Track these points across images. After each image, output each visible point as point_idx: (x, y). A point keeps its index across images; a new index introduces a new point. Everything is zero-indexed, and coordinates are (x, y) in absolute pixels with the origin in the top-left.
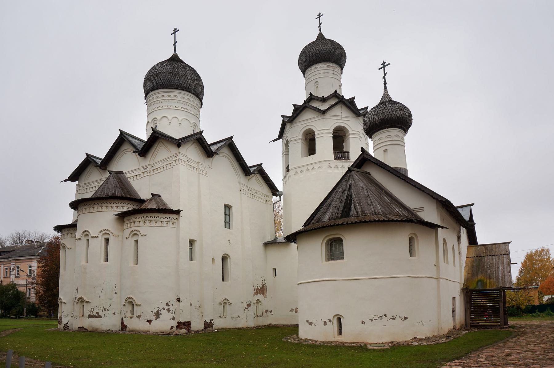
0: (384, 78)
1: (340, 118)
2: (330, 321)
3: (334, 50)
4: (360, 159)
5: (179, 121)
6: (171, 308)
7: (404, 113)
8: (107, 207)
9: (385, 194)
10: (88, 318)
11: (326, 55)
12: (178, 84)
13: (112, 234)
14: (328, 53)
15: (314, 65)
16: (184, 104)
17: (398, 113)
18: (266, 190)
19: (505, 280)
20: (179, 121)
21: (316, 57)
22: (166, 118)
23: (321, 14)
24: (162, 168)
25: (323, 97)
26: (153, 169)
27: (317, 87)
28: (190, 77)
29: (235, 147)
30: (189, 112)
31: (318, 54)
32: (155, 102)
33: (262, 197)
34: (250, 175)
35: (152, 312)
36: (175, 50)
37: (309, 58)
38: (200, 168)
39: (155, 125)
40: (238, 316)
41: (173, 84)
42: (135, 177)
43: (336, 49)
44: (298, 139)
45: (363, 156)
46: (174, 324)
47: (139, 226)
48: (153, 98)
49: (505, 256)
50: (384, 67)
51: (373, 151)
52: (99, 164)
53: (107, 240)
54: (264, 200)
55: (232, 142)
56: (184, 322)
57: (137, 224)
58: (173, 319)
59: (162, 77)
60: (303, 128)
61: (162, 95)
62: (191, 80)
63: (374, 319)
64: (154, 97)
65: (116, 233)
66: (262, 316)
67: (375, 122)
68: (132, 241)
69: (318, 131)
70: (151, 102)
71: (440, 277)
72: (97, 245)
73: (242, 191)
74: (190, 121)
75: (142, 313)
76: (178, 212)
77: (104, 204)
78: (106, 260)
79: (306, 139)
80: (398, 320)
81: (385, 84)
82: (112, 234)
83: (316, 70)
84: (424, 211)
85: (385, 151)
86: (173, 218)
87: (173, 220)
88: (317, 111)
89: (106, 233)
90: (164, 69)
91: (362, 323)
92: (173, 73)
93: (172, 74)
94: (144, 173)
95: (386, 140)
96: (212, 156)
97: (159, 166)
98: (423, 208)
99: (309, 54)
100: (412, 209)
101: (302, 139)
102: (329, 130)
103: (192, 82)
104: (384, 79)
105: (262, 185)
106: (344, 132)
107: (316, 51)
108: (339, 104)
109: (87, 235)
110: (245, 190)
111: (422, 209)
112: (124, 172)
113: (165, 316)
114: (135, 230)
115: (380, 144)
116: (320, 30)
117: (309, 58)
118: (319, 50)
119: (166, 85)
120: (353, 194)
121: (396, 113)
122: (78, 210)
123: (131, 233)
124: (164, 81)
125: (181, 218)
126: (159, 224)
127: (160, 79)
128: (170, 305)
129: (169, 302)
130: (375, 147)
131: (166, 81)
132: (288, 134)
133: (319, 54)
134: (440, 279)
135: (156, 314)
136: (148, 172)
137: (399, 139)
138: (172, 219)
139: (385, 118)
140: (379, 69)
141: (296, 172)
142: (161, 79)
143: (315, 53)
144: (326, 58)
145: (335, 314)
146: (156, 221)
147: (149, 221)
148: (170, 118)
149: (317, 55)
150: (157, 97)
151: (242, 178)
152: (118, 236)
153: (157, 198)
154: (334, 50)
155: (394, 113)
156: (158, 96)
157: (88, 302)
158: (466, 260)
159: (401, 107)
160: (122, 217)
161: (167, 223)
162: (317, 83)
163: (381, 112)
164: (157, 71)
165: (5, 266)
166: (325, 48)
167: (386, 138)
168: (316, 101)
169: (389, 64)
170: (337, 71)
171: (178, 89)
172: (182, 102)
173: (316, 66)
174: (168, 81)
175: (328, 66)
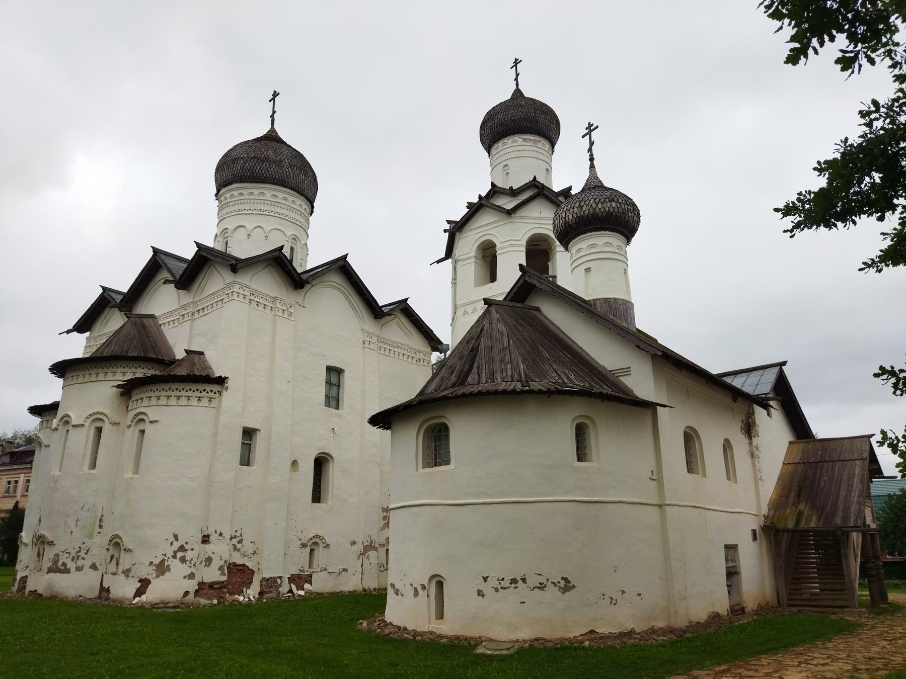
1: (538, 221)
2: (423, 587)
4: (519, 285)
5: (265, 233)
6: (189, 555)
7: (618, 205)
8: (106, 373)
10: (47, 573)
11: (522, 122)
12: (266, 176)
13: (109, 419)
15: (502, 139)
16: (262, 203)
17: (606, 205)
18: (417, 342)
20: (265, 233)
21: (505, 126)
22: (243, 228)
26: (198, 309)
28: (287, 164)
29: (352, 272)
30: (285, 218)
31: (508, 122)
32: (229, 204)
33: (409, 354)
34: (383, 317)
35: (151, 563)
37: (494, 129)
38: (279, 306)
39: (226, 240)
41: (258, 175)
43: (538, 112)
44: (469, 258)
45: (525, 280)
46: (192, 585)
47: (158, 404)
48: (226, 197)
50: (589, 133)
52: (118, 302)
53: (99, 430)
54: (415, 360)
55: (345, 263)
56: (211, 583)
58: (191, 576)
59: (240, 164)
60: (477, 240)
62: (290, 169)
63: (502, 588)
64: (228, 195)
65: (115, 419)
68: (134, 432)
69: (501, 243)
70: (223, 204)
71: (668, 502)
72: (81, 440)
73: (367, 345)
74: (285, 232)
77: (101, 369)
78: (93, 466)
79: (484, 257)
80: (552, 592)
81: (592, 159)
82: (109, 419)
84: (630, 374)
85: (588, 270)
86: (212, 391)
87: (211, 395)
88: (499, 211)
89: (97, 419)
90: (245, 153)
91: (479, 595)
92: (258, 158)
94: (184, 315)
95: (587, 253)
96: (302, 287)
97: (207, 305)
100: (610, 371)
101: (476, 257)
102: (519, 240)
103: (291, 171)
106: (549, 243)
107: (504, 117)
110: (373, 343)
111: (627, 371)
112: (156, 315)
113: (178, 569)
114: (141, 413)
115: (580, 259)
116: (517, 85)
117: (494, 129)
118: (509, 116)
120: (483, 345)
124: (244, 171)
125: (224, 393)
126: (183, 401)
127: (237, 169)
128: (187, 550)
129: (187, 543)
130: (573, 264)
132: (457, 252)
134: (666, 507)
136: (190, 314)
137: (612, 250)
138: (209, 392)
139: (584, 216)
141: (465, 311)
143: (503, 121)
144: (522, 126)
147: (167, 396)
148: (250, 227)
150: (232, 196)
151: (368, 323)
152: (119, 424)
153: (196, 359)
154: (534, 115)
155: (600, 206)
156: (232, 194)
157: (51, 543)
158: (782, 469)
160: (128, 390)
161: (199, 399)
163: (577, 204)
164: (233, 155)
165: (26, 477)
166: (519, 111)
167: (604, 246)
168: (502, 195)
169: (598, 126)
170: (542, 147)
172: (273, 203)
173: (505, 140)
175: (525, 140)
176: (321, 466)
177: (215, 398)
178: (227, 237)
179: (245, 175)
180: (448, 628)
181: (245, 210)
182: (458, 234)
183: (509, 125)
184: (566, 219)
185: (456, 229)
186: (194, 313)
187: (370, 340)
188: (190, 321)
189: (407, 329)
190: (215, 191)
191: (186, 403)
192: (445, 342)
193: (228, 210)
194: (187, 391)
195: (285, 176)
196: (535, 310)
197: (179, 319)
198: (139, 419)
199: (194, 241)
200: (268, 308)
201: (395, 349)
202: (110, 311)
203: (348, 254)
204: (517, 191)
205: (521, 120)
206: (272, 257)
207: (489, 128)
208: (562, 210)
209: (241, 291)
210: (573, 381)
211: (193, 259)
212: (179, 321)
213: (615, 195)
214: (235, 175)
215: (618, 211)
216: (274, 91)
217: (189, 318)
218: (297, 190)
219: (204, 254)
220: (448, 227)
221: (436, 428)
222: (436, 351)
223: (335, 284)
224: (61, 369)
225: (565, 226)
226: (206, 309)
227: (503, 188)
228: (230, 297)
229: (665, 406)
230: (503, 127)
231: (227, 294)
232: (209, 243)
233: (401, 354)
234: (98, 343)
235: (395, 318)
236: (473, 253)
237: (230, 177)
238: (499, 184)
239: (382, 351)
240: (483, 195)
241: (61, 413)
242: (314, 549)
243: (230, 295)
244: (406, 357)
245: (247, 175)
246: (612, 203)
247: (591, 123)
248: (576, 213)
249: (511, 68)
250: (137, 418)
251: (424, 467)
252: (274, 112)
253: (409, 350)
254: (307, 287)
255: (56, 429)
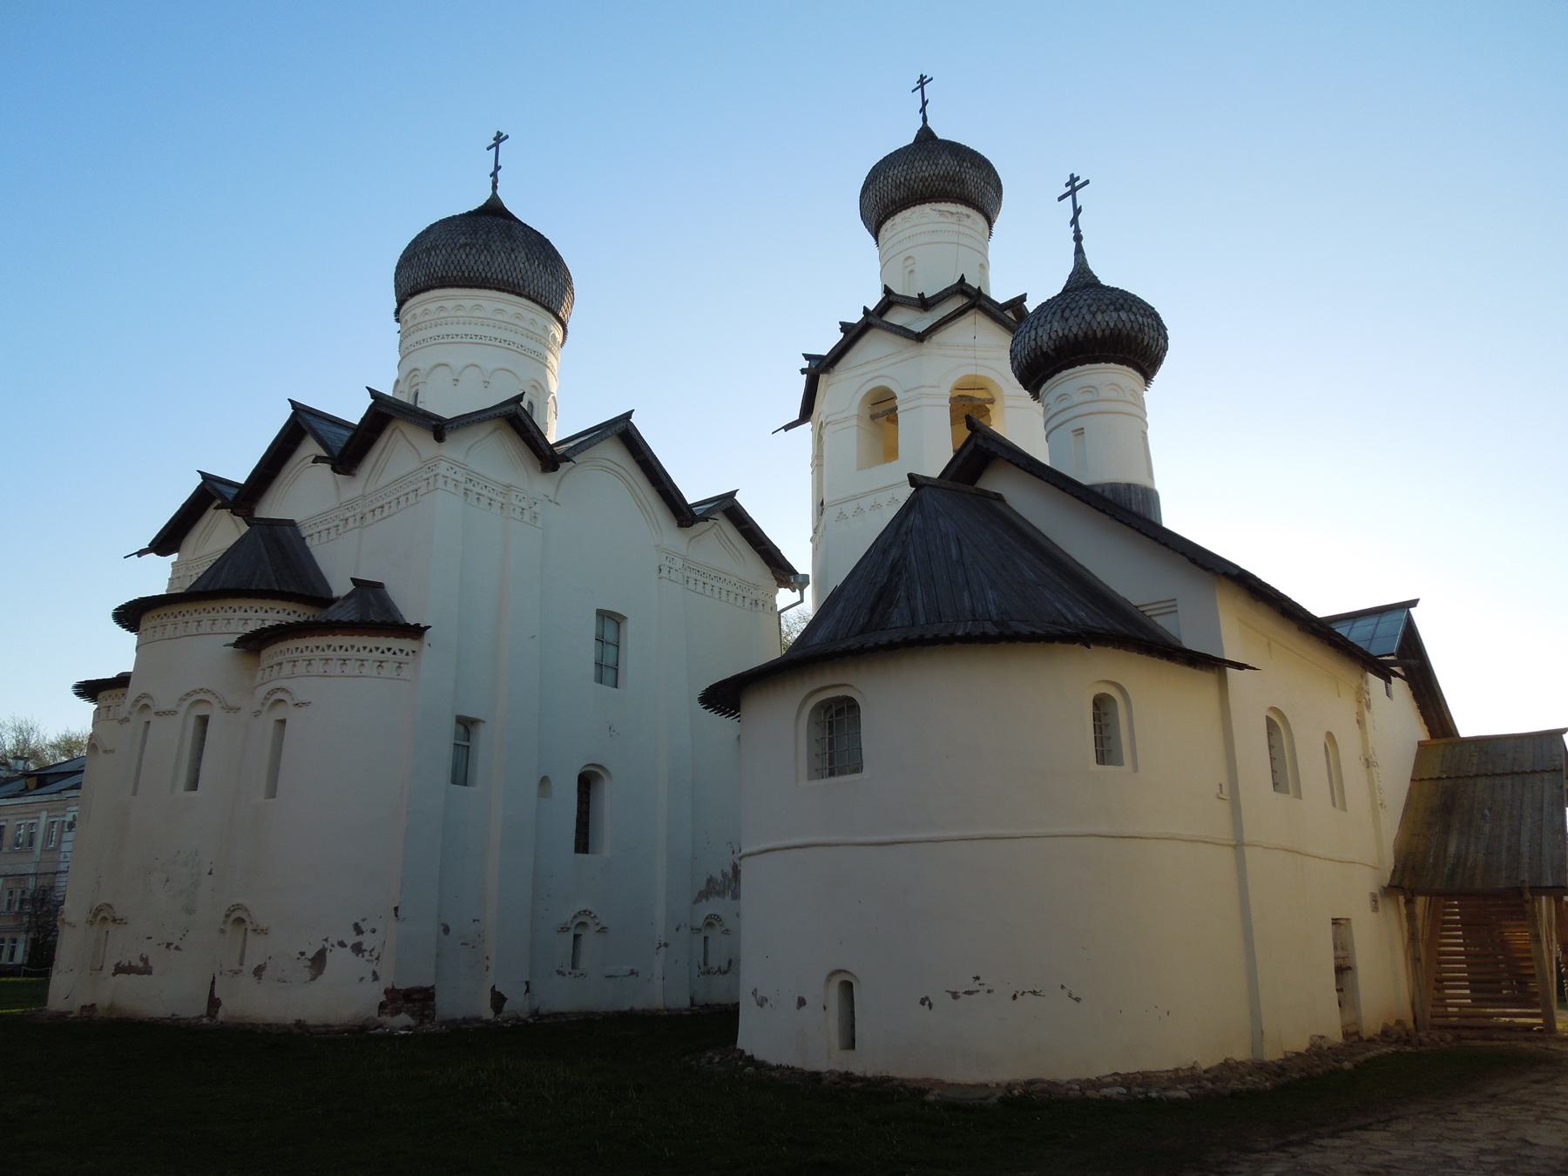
0: (1074, 221)
3: (957, 169)
6: (368, 941)
9: (304, 426)
10: (114, 975)
11: (937, 183)
14: (941, 178)
17: (1111, 316)
19: (1540, 861)
23: (926, 77)
24: (394, 504)
25: (921, 295)
27: (911, 271)
31: (912, 183)
32: (419, 326)
35: (302, 954)
36: (495, 187)
40: (633, 973)
42: (324, 534)
46: (376, 993)
49: (1546, 776)
50: (1073, 192)
51: (1045, 433)
52: (230, 499)
53: (204, 721)
57: (287, 668)
61: (440, 305)
63: (968, 993)
66: (725, 972)
67: (1041, 347)
73: (665, 573)
75: (270, 958)
76: (417, 632)
78: (193, 785)
81: (1078, 238)
83: (907, 225)
84: (1176, 611)
86: (401, 651)
89: (197, 697)
93: (471, 249)
96: (555, 468)
97: (388, 500)
98: (1174, 603)
99: (885, 182)
103: (528, 267)
104: (1073, 226)
105: (741, 555)
107: (904, 173)
108: (970, 312)
109: (146, 706)
112: (297, 520)
116: (925, 119)
119: (452, 279)
121: (1103, 317)
122: (141, 629)
123: (268, 699)
124: (447, 267)
130: (1049, 424)
131: (452, 267)
133: (915, 182)
135: (313, 960)
136: (358, 517)
138: (398, 652)
139: (1071, 335)
140: (1060, 199)
142: (439, 263)
143: (902, 180)
144: (937, 190)
145: (833, 968)
146: (345, 660)
149: (909, 184)
150: (426, 312)
154: (957, 169)
156: (426, 310)
159: (1121, 301)
160: (253, 644)
162: (910, 262)
167: (1080, 391)
171: (485, 288)
174: (458, 268)
176: (589, 789)
177: (407, 663)
178: (418, 384)
179: (450, 275)
180: (866, 1062)
181: (505, 341)
182: (823, 378)
183: (913, 188)
184: (1036, 342)
185: (819, 368)
186: (364, 514)
187: (671, 565)
188: (356, 531)
189: (734, 546)
190: (395, 305)
191: (357, 672)
192: (800, 571)
193: (418, 336)
194: (358, 650)
195: (519, 277)
196: (995, 500)
197: (337, 526)
198: (275, 701)
199: (367, 388)
200: (496, 506)
201: (714, 583)
202: (214, 514)
203: (633, 410)
204: (932, 301)
205: (934, 178)
206: (504, 414)
207: (878, 194)
208: (1029, 326)
209: (450, 474)
210: (1082, 615)
211: (248, 481)
212: (338, 530)
213: (1124, 301)
214: (431, 277)
215: (1132, 327)
216: (498, 132)
217: (357, 524)
218: (539, 300)
219: (384, 410)
220: (806, 364)
221: (831, 707)
222: (786, 588)
223: (609, 464)
224: (131, 615)
225: (1036, 354)
226: (386, 507)
227: (907, 297)
228: (432, 484)
229: (1241, 666)
230: (902, 190)
231: (425, 480)
232: (387, 390)
233: (724, 593)
234: (193, 572)
235: (713, 526)
236: (854, 410)
237: (423, 279)
238: (898, 290)
239: (691, 585)
240: (871, 308)
241: (133, 691)
242: (580, 935)
243: (431, 481)
244: (732, 597)
245: (452, 275)
246: (1121, 313)
247: (1075, 176)
248: (1056, 331)
249: (913, 91)
250: (272, 700)
251: (810, 778)
252: (497, 168)
253: (738, 585)
254: (564, 466)
255: (126, 720)
